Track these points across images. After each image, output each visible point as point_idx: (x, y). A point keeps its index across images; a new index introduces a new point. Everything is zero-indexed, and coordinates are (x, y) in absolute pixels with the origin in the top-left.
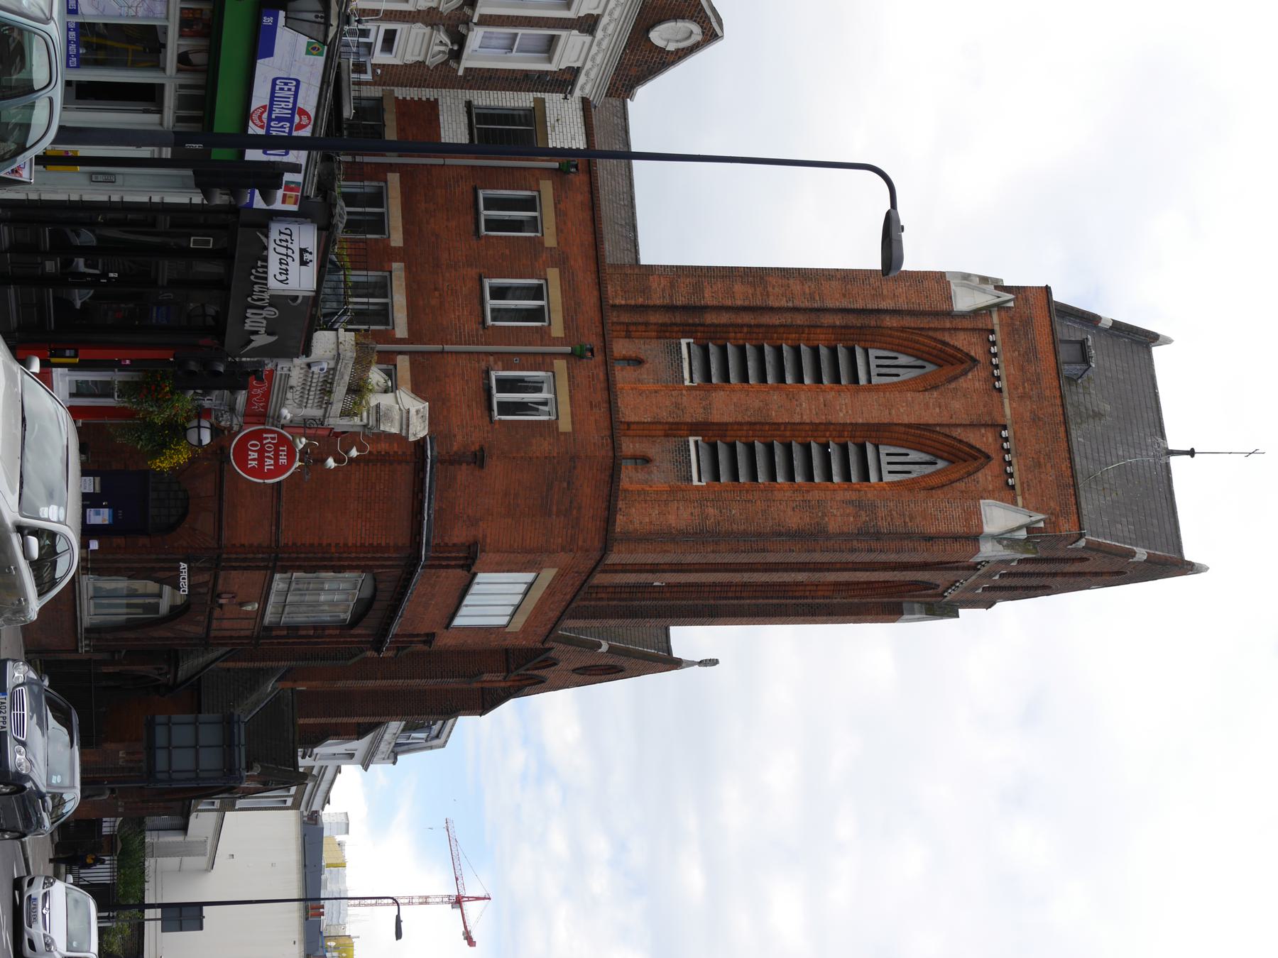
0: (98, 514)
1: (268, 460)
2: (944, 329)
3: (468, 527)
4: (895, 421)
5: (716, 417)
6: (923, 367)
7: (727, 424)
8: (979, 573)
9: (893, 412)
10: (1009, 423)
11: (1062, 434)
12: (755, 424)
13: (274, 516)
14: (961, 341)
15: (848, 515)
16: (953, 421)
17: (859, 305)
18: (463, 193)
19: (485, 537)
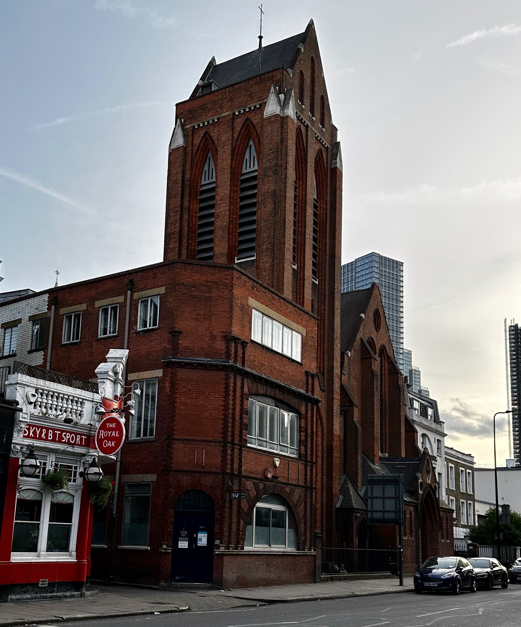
0: (201, 540)
1: (113, 434)
2: (192, 150)
3: (216, 341)
4: (230, 166)
5: (225, 251)
6: (209, 158)
7: (229, 245)
8: (309, 124)
9: (226, 167)
10: (232, 112)
11: (238, 86)
12: (229, 232)
13: (204, 443)
14: (197, 141)
15: (269, 180)
16: (231, 138)
17: (180, 189)
18: (63, 352)
19: (222, 332)
